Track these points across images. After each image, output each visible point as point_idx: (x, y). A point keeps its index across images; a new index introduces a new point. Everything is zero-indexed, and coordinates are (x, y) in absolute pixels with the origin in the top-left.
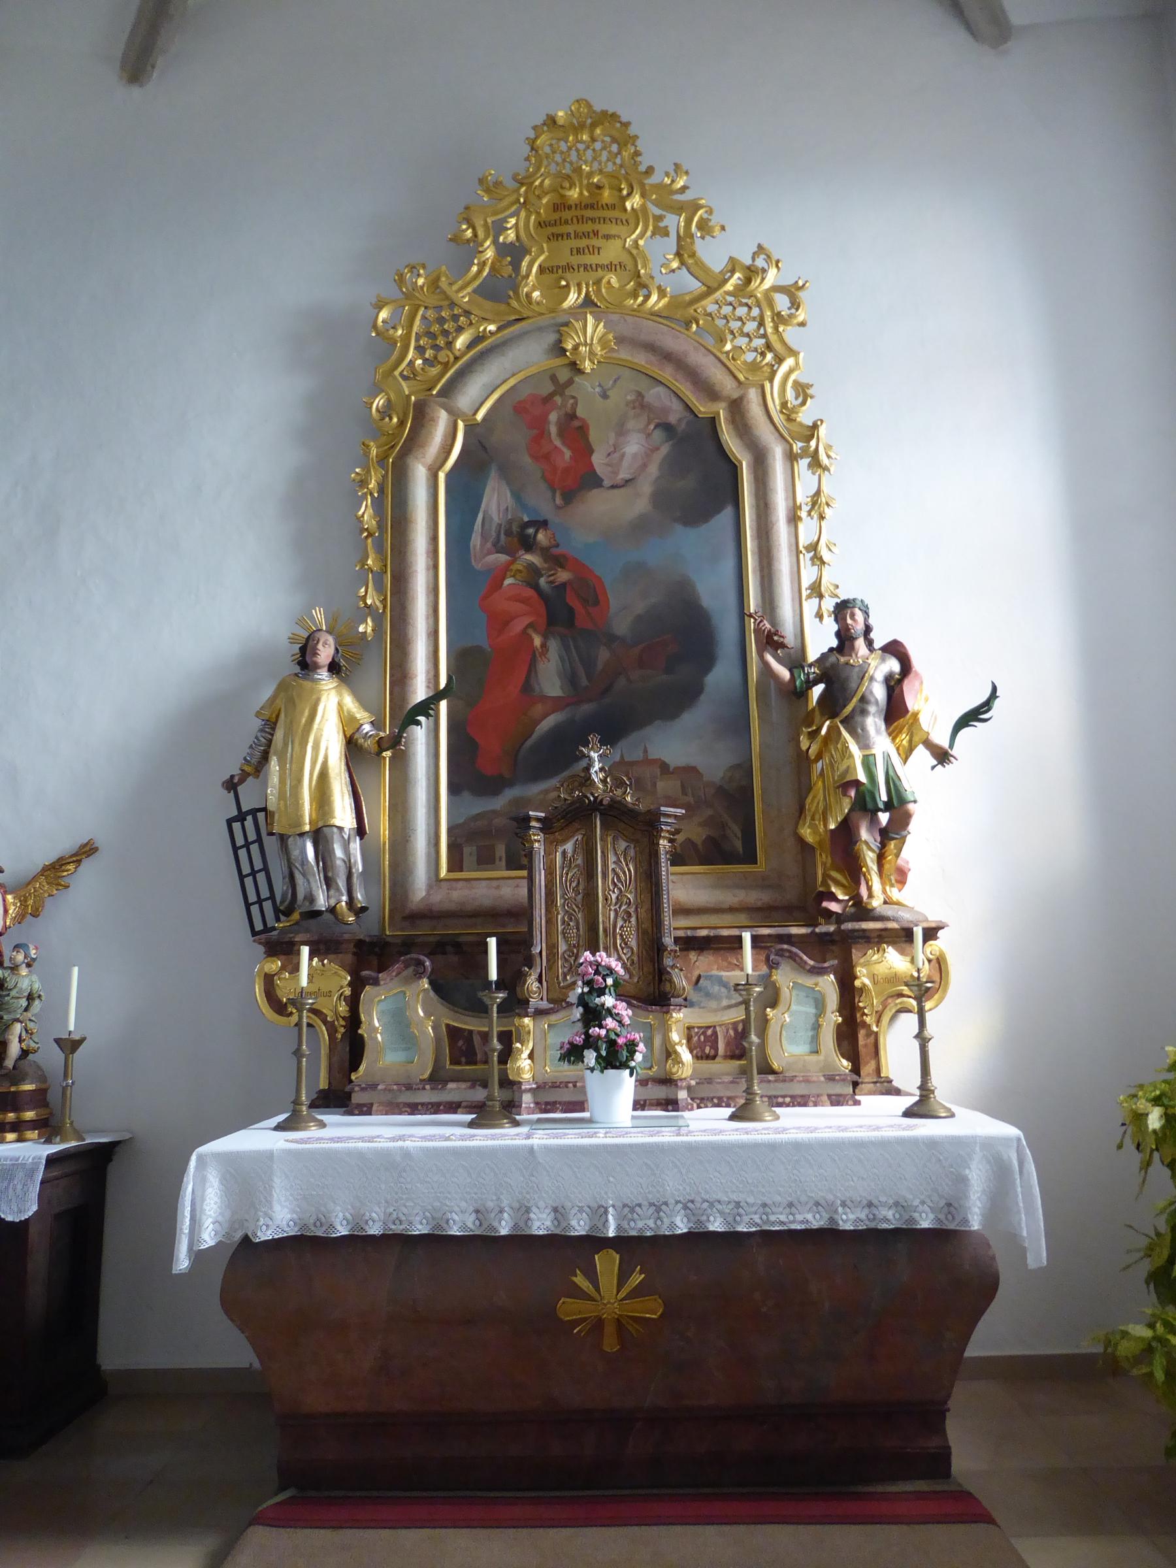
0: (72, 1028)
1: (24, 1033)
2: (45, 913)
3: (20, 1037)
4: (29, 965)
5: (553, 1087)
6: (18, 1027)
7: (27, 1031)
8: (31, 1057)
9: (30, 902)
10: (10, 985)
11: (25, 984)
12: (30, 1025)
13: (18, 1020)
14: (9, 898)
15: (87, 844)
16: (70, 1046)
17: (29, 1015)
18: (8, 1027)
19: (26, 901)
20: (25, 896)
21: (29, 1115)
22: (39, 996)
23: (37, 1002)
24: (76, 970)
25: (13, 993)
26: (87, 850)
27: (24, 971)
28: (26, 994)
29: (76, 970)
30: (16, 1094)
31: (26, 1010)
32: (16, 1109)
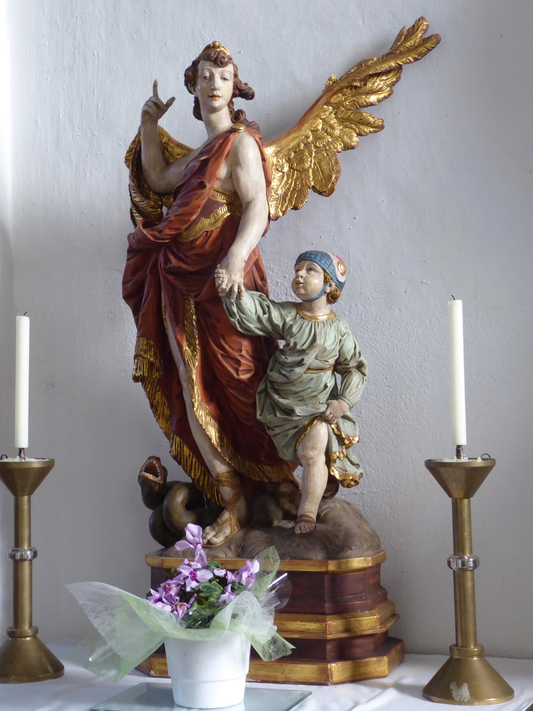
0: (462, 440)
1: (335, 447)
2: (341, 186)
3: (328, 453)
4: (332, 298)
5: (378, 546)
6: (322, 430)
7: (341, 440)
8: (342, 492)
9: (309, 163)
10: (302, 340)
11: (328, 340)
12: (346, 428)
13: (322, 417)
14: (269, 151)
15: (413, 30)
16: (460, 479)
17: (340, 406)
18: (302, 432)
19: (301, 161)
20: (296, 150)
21: (369, 622)
22: (360, 366)
23: (356, 378)
24: (24, 324)
25: (310, 359)
26: (412, 45)
27: (323, 311)
28: (332, 361)
29: (24, 324)
30: (337, 578)
31: (335, 394)
32: (342, 610)
